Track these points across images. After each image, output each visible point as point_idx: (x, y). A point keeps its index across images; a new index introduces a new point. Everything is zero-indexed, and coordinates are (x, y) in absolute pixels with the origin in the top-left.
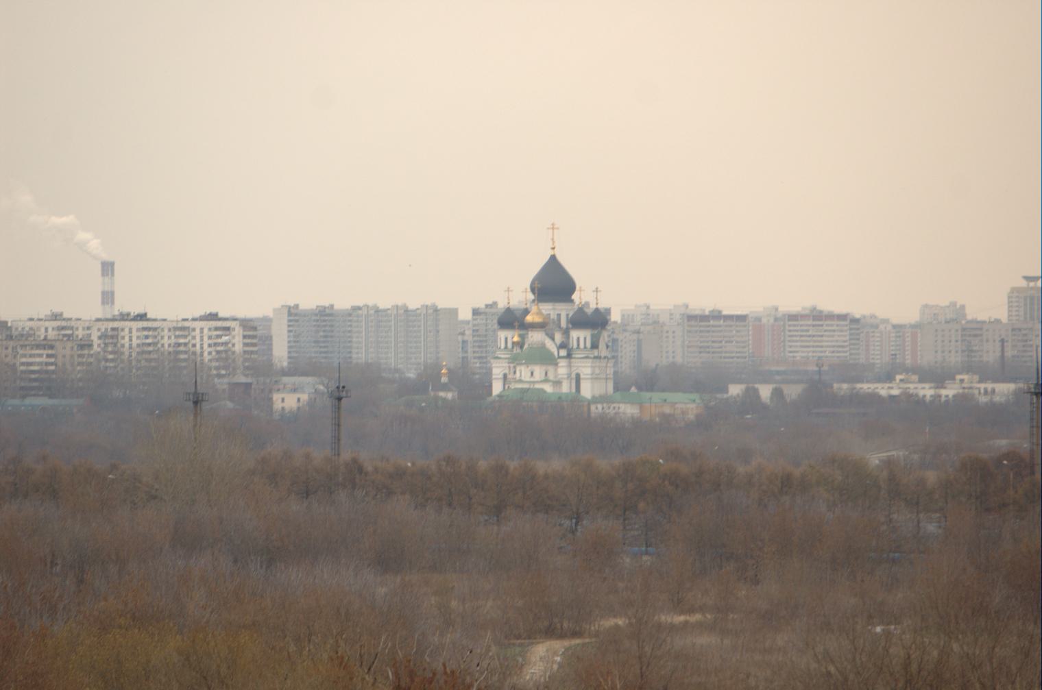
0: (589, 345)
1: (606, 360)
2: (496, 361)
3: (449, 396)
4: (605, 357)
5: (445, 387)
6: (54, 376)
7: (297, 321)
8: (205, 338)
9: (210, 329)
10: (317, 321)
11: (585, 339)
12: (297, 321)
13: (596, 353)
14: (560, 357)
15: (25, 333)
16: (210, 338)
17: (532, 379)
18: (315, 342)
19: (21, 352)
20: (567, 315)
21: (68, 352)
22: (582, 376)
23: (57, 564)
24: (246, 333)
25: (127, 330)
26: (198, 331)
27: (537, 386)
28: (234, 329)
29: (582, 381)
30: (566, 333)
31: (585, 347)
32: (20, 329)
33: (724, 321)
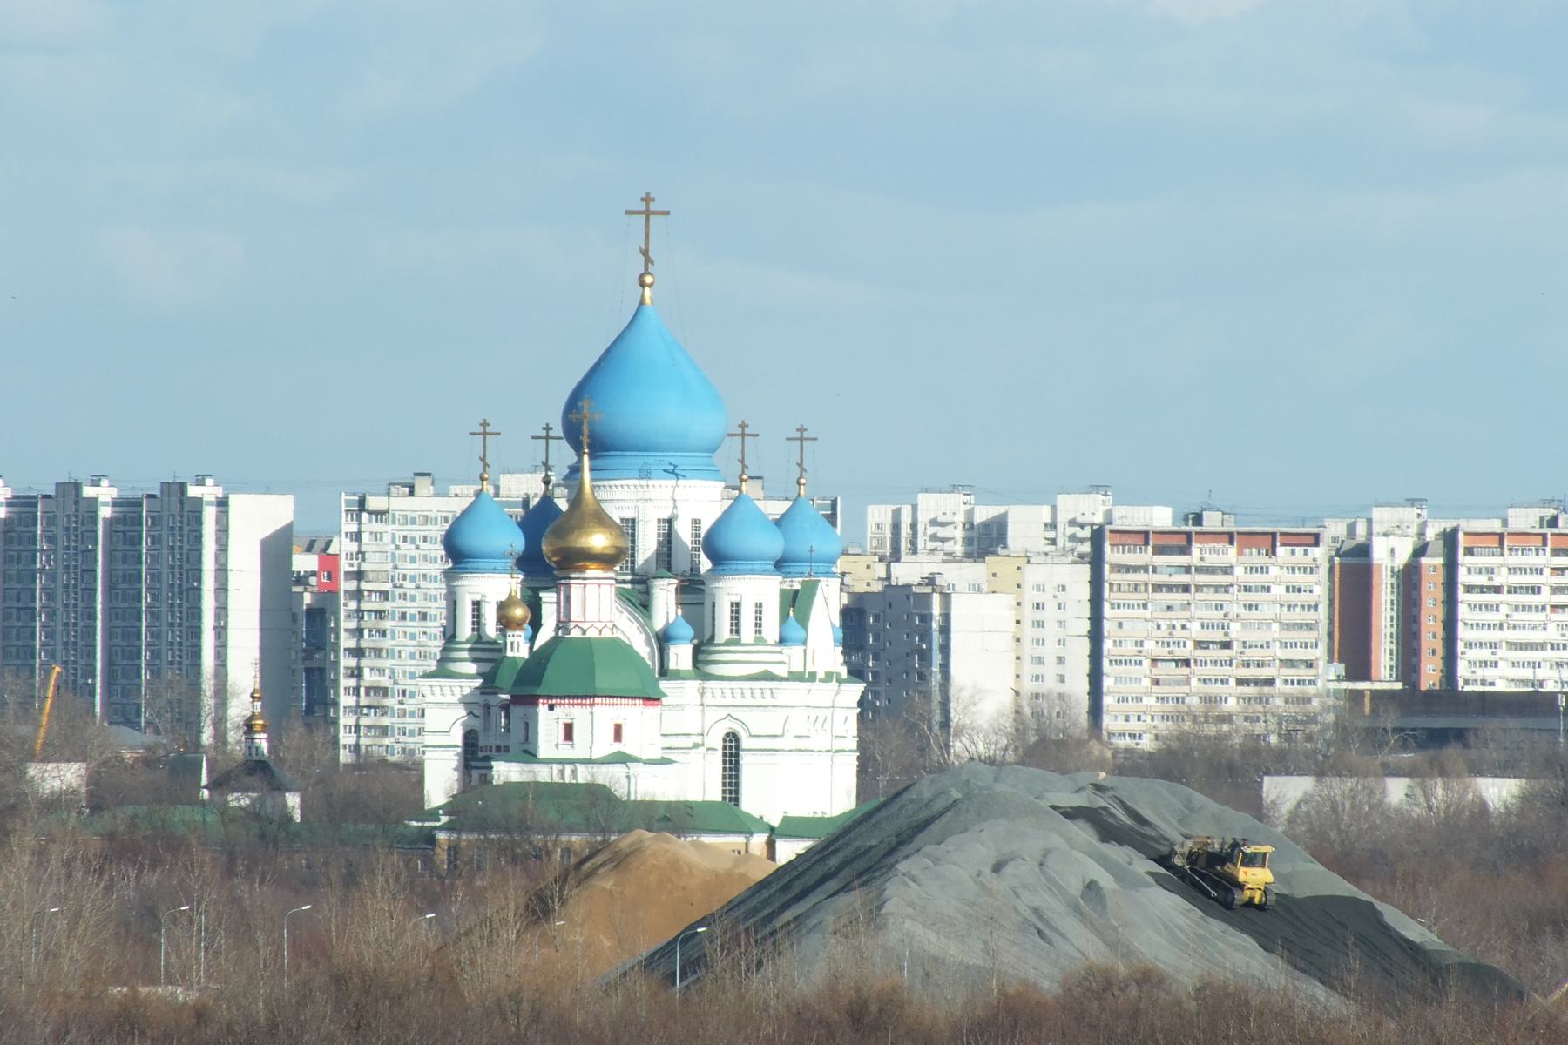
0: (771, 630)
1: (834, 684)
4: (829, 677)
11: (759, 606)
13: (793, 657)
17: (565, 752)
20: (696, 523)
22: (745, 743)
27: (583, 775)
31: (759, 641)
33: (1240, 553)
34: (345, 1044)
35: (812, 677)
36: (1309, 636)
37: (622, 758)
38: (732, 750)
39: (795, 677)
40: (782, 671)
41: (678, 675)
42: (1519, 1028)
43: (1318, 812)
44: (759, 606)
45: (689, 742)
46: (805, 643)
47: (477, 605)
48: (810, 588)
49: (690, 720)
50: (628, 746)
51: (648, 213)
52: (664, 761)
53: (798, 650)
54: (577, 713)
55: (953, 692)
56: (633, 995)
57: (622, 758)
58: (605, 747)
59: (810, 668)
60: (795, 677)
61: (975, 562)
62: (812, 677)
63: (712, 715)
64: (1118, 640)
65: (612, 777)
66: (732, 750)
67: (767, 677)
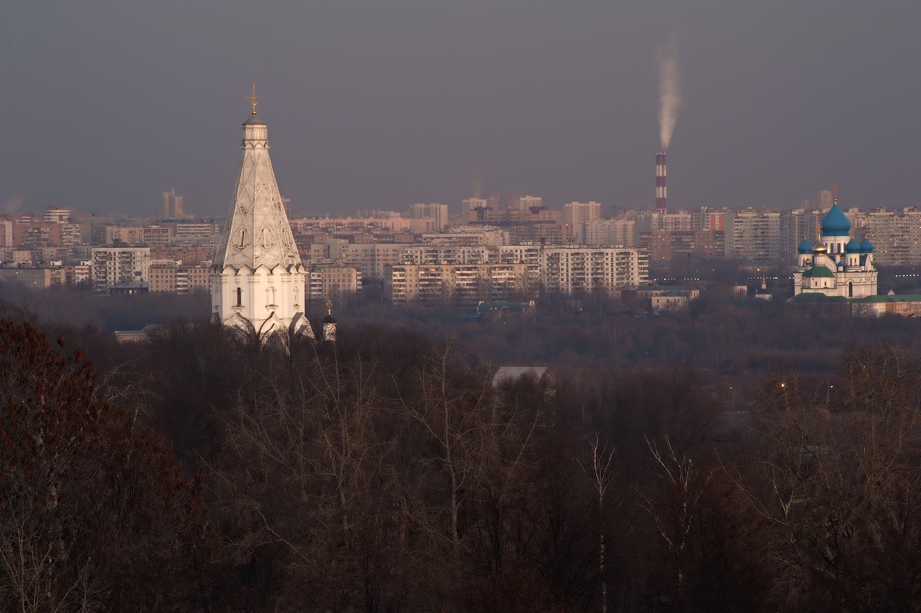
1: (871, 273)
2: (797, 274)
3: (767, 296)
4: (870, 271)
5: (764, 292)
6: (513, 287)
7: (740, 222)
8: (614, 260)
9: (617, 254)
10: (757, 221)
11: (855, 259)
12: (740, 222)
13: (863, 268)
14: (838, 272)
15: (507, 253)
16: (617, 259)
17: (816, 287)
18: (754, 237)
19: (493, 272)
20: (845, 244)
21: (522, 271)
22: (853, 284)
23: (72, 426)
24: (639, 256)
25: (565, 254)
26: (610, 255)
27: (820, 291)
28: (632, 254)
29: (853, 287)
30: (843, 256)
32: (504, 251)
37: (826, 288)
38: (851, 285)
39: (863, 271)
40: (860, 271)
41: (840, 272)
42: (174, 543)
43: (126, 341)
44: (855, 259)
45: (843, 284)
46: (864, 265)
47: (851, 259)
49: (843, 280)
52: (835, 288)
53: (863, 267)
56: (226, 436)
57: (826, 288)
58: (823, 286)
59: (866, 270)
60: (863, 271)
61: (175, 208)
63: (847, 279)
64: (342, 249)
65: (824, 292)
66: (851, 285)
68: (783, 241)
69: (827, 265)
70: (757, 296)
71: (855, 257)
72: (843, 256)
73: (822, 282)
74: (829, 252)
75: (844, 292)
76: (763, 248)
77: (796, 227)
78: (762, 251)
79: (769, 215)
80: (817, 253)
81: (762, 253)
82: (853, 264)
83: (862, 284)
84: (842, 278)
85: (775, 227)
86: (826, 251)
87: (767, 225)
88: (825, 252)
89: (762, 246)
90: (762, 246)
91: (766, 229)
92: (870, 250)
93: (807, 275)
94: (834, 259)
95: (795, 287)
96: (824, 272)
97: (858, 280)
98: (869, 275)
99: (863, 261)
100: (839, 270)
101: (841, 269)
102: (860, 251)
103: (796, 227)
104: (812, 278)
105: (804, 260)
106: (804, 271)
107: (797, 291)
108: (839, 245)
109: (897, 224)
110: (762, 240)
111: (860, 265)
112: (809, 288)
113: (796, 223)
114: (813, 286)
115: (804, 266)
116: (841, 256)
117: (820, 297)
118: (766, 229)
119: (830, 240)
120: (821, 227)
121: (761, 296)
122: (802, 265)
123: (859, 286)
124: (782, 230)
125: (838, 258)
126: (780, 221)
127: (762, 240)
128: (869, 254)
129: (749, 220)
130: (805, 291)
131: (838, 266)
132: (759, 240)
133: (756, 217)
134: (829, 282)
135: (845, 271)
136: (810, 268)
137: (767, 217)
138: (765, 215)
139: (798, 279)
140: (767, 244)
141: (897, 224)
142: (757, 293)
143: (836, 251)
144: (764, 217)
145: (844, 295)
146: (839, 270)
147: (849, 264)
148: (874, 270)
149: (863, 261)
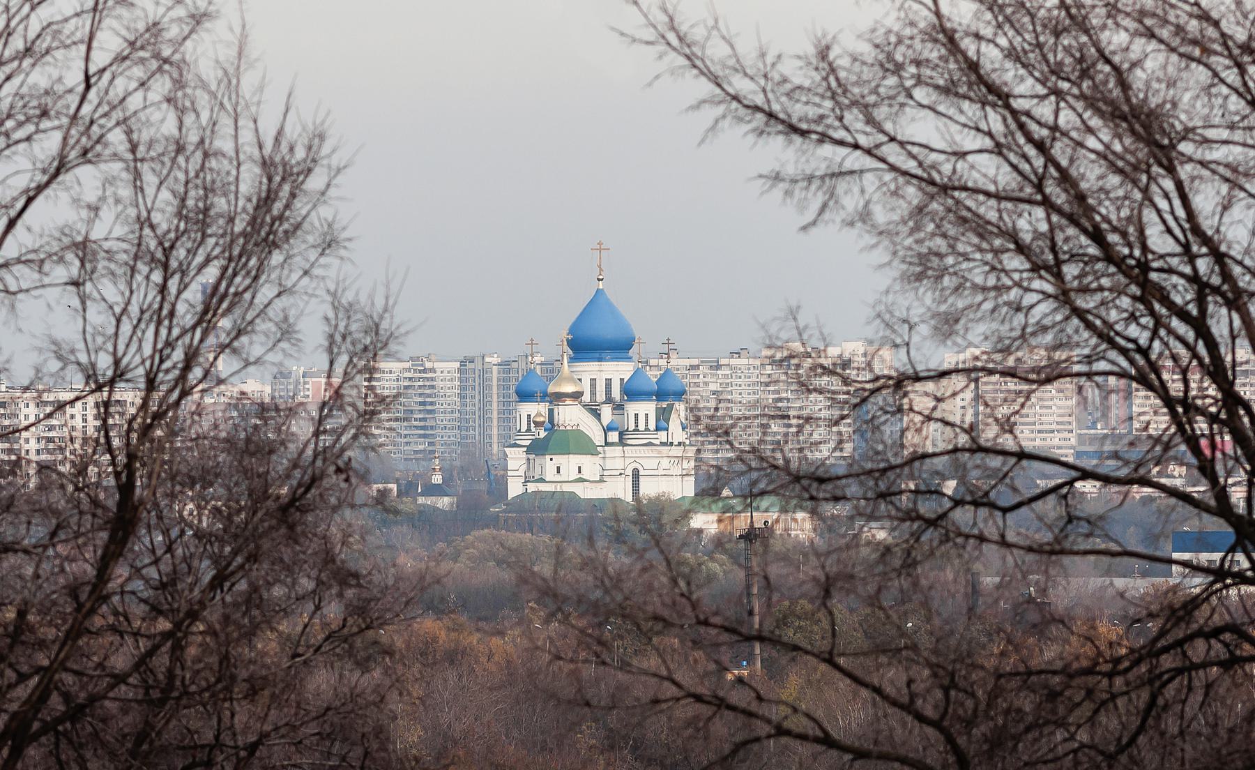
0: (652, 426)
3: (444, 502)
4: (680, 444)
10: (410, 379)
13: (662, 436)
14: (607, 444)
17: (558, 478)
20: (622, 380)
27: (567, 488)
29: (641, 479)
30: (618, 407)
31: (647, 429)
34: (2, 411)
35: (671, 444)
36: (1070, 419)
38: (636, 475)
39: (663, 444)
40: (657, 442)
41: (612, 444)
46: (667, 429)
47: (636, 415)
48: (671, 407)
49: (618, 464)
50: (585, 475)
51: (600, 250)
52: (601, 481)
54: (559, 459)
55: (991, 455)
58: (574, 476)
60: (663, 444)
62: (671, 444)
63: (628, 461)
66: (636, 475)
67: (650, 444)
68: (467, 421)
69: (581, 428)
70: (421, 500)
71: (646, 409)
72: (618, 407)
73: (570, 464)
74: (586, 398)
75: (620, 490)
76: (425, 436)
77: (495, 390)
78: (421, 443)
79: (436, 365)
80: (559, 397)
81: (421, 447)
82: (642, 427)
83: (661, 472)
84: (616, 458)
85: (449, 392)
86: (581, 394)
87: (433, 387)
88: (577, 396)
89: (422, 432)
90: (422, 432)
91: (429, 396)
92: (679, 395)
93: (538, 448)
94: (597, 415)
95: (510, 480)
96: (576, 443)
97: (652, 463)
98: (677, 451)
99: (663, 417)
100: (610, 434)
101: (614, 437)
102: (660, 395)
103: (495, 390)
104: (548, 457)
105: (529, 416)
106: (528, 443)
107: (515, 489)
108: (609, 382)
109: (706, 384)
110: (421, 420)
111: (658, 429)
112: (542, 480)
113: (495, 382)
114: (550, 474)
115: (529, 430)
116: (613, 409)
117: (566, 505)
118: (429, 396)
119: (589, 370)
120: (570, 337)
121: (429, 501)
122: (524, 428)
123: (656, 479)
124: (465, 397)
125: (607, 413)
126: (460, 379)
127: (421, 420)
128: (677, 404)
129: (393, 376)
130: (532, 487)
131: (607, 430)
132: (416, 420)
133: (409, 370)
134: (590, 465)
135: (622, 442)
136: (543, 434)
137: (433, 370)
138: (428, 365)
139: (516, 460)
140: (432, 428)
141: (706, 384)
142: (422, 494)
143: (601, 396)
144: (425, 371)
145: (621, 496)
146: (610, 440)
147: (632, 427)
148: (687, 442)
149: (663, 417)
